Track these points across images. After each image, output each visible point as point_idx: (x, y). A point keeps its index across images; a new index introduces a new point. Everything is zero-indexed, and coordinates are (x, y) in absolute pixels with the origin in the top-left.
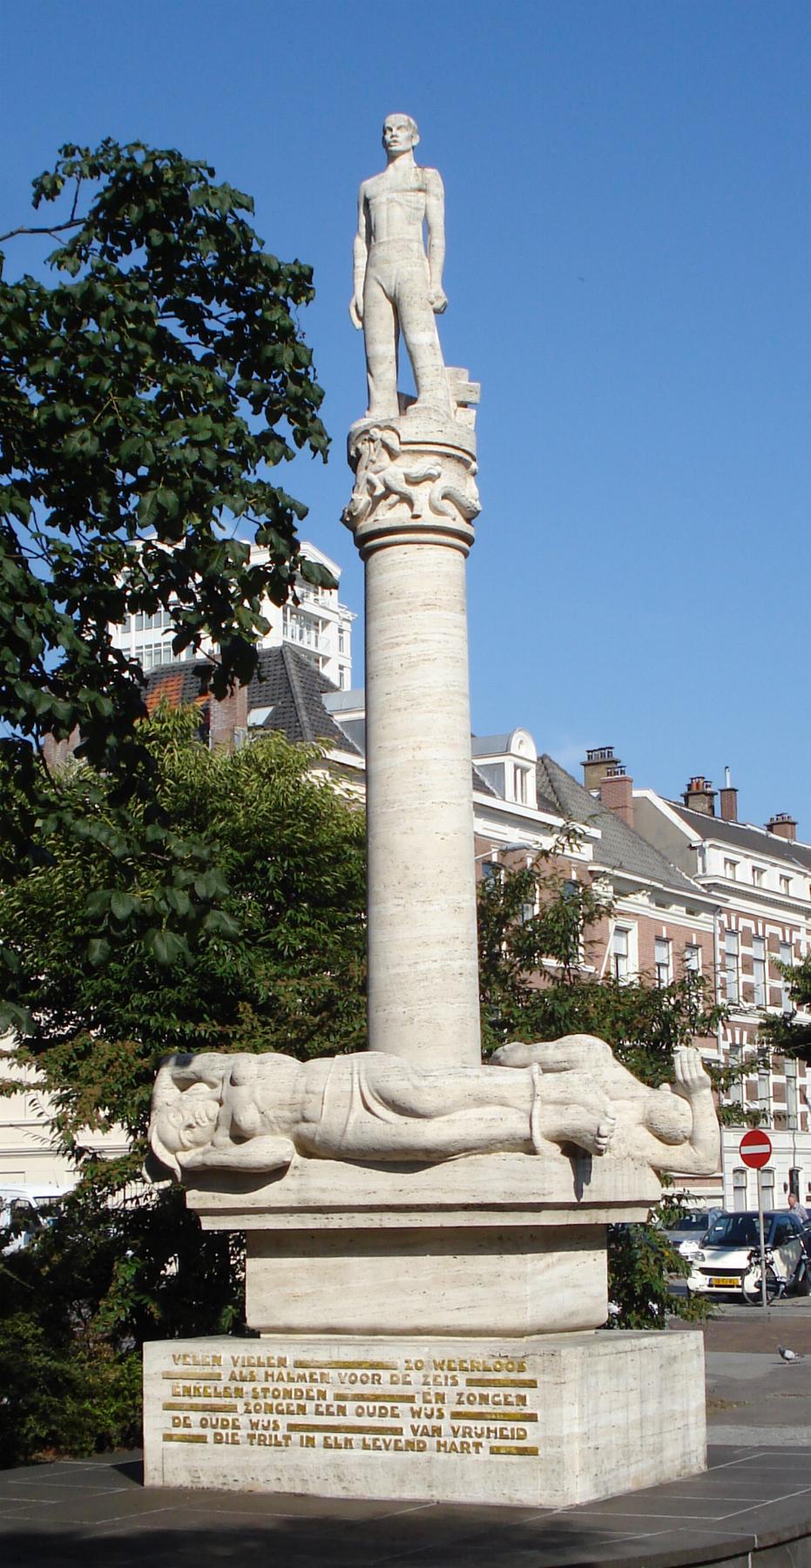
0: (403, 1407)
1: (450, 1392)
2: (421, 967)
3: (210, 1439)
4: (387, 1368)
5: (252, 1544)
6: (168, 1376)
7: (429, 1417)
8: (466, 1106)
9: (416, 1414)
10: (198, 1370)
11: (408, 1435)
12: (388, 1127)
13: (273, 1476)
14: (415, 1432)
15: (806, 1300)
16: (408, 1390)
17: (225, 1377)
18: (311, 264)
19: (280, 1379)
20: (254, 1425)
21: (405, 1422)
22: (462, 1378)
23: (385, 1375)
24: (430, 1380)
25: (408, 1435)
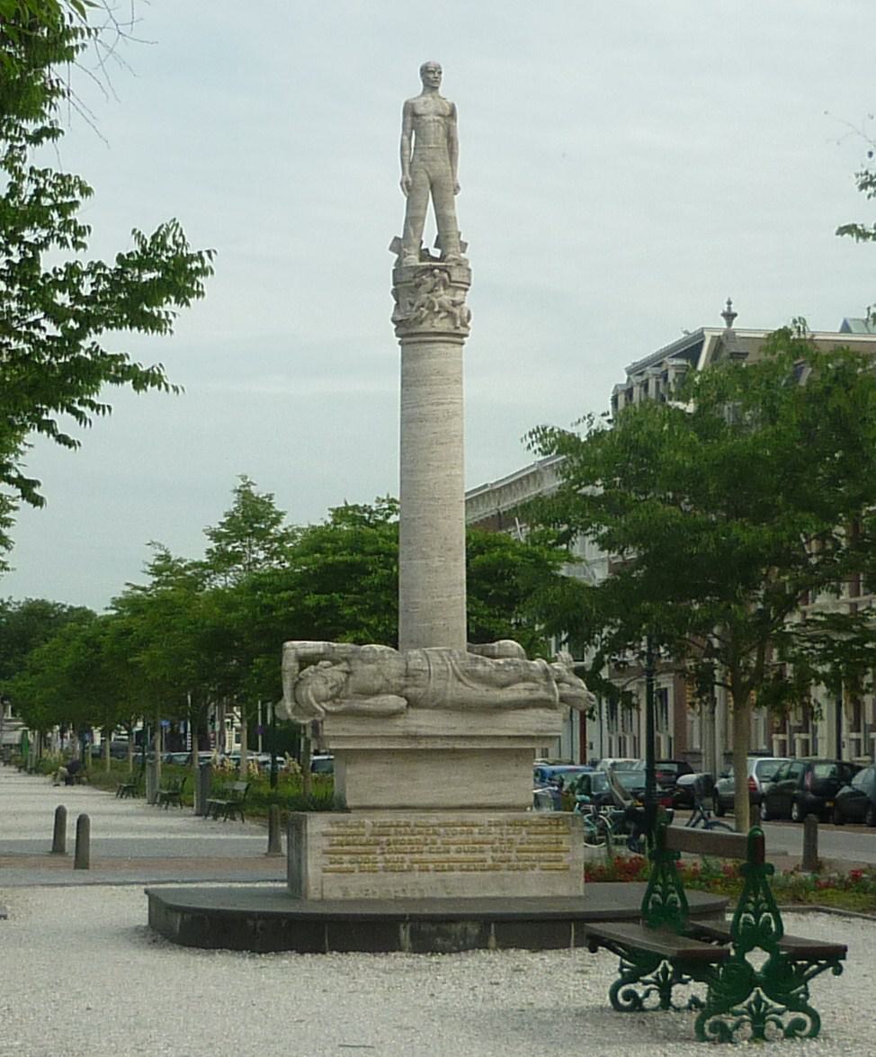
0: (486, 847)
1: (517, 838)
2: (453, 598)
3: (357, 871)
4: (477, 826)
5: (773, 925)
6: (325, 835)
7: (503, 852)
8: (519, 682)
9: (495, 851)
10: (349, 831)
11: (490, 862)
12: (475, 692)
13: (399, 889)
14: (494, 860)
15: (4, 742)
16: (491, 838)
17: (367, 835)
18: (460, 185)
19: (405, 834)
20: (387, 861)
21: (488, 856)
22: (524, 830)
23: (476, 830)
24: (504, 832)
25: (490, 862)
